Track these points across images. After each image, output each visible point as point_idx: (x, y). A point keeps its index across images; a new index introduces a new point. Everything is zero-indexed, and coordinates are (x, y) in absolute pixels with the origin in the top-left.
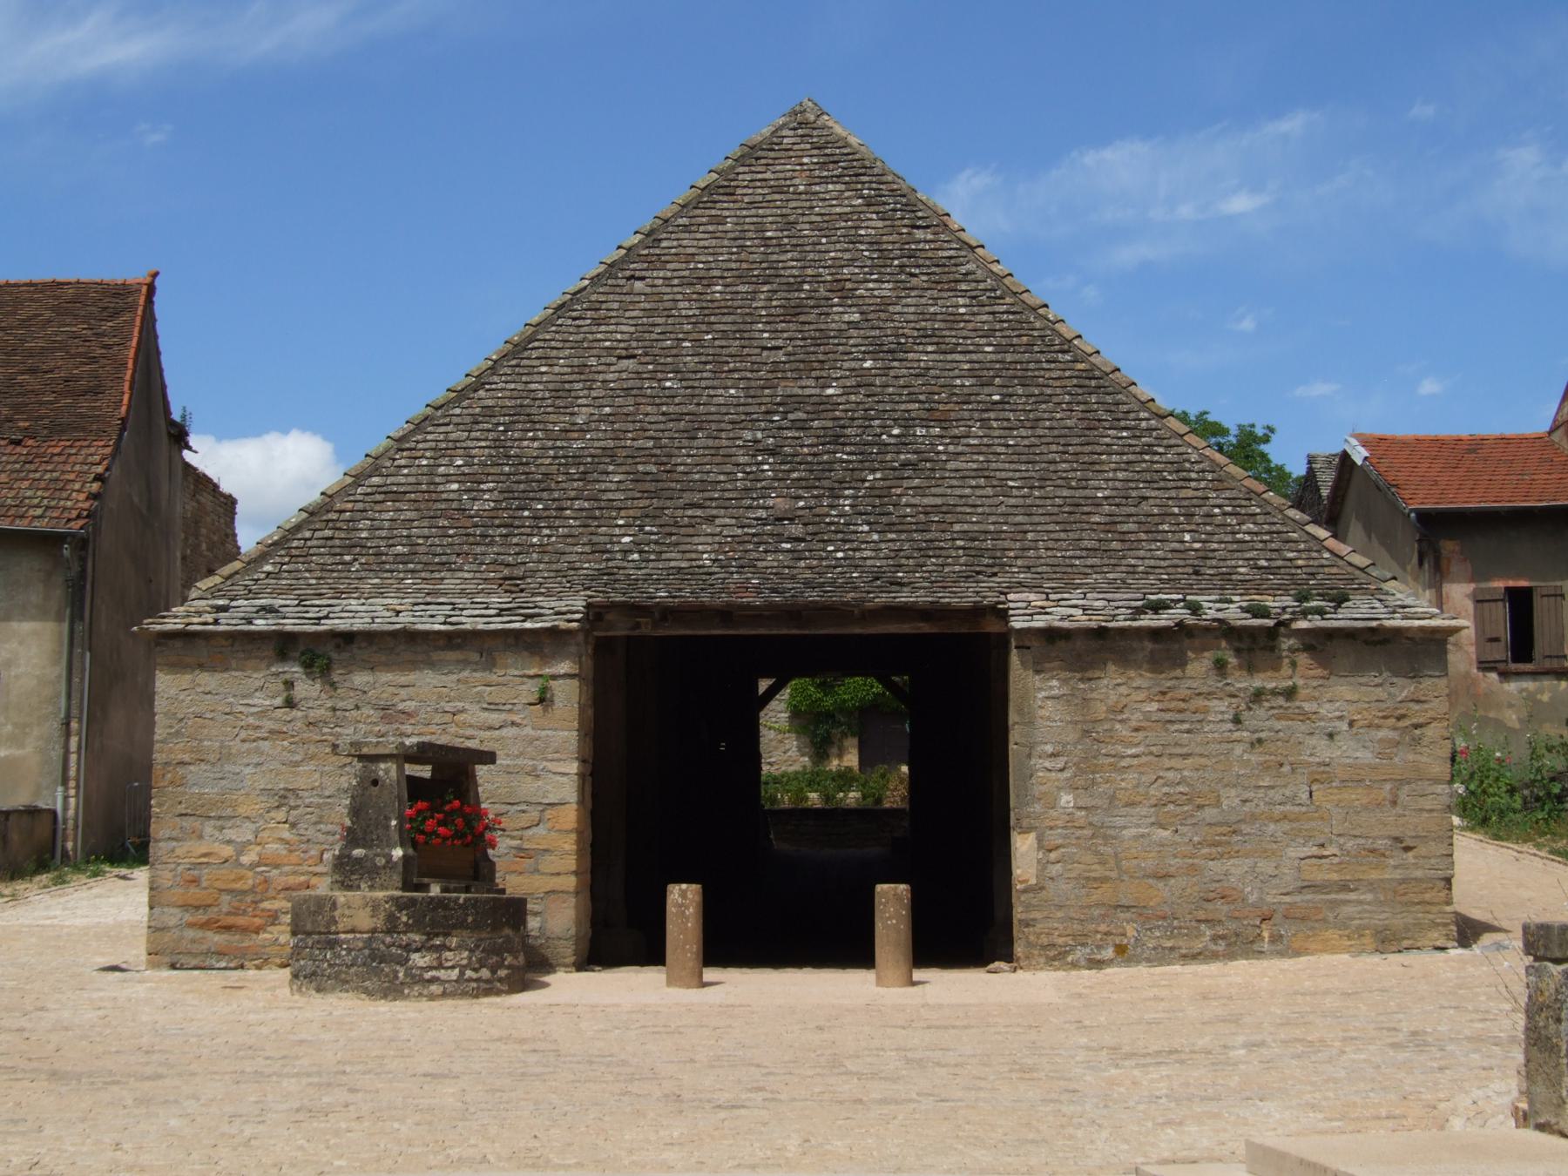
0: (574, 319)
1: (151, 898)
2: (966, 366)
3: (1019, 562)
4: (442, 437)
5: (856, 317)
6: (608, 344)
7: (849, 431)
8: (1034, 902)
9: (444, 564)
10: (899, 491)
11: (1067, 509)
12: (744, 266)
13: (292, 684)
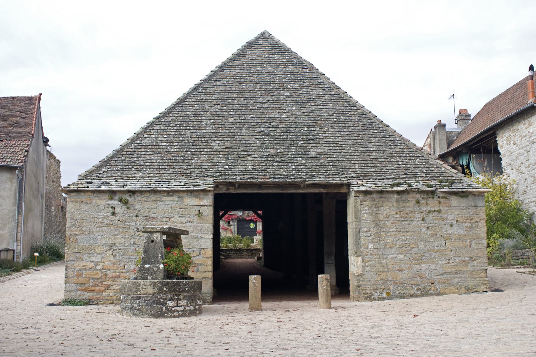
0: (199, 93)
1: (66, 281)
2: (325, 110)
3: (351, 170)
4: (159, 128)
5: (288, 94)
6: (210, 100)
7: (291, 129)
8: (361, 279)
9: (163, 169)
10: (309, 147)
11: (362, 154)
12: (252, 78)
13: (114, 208)
